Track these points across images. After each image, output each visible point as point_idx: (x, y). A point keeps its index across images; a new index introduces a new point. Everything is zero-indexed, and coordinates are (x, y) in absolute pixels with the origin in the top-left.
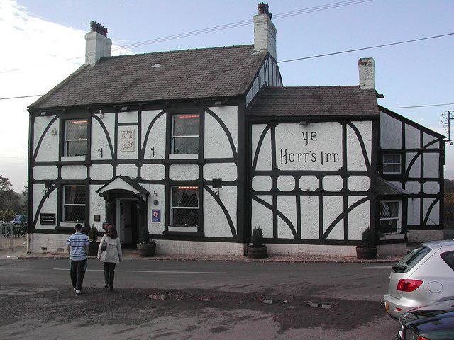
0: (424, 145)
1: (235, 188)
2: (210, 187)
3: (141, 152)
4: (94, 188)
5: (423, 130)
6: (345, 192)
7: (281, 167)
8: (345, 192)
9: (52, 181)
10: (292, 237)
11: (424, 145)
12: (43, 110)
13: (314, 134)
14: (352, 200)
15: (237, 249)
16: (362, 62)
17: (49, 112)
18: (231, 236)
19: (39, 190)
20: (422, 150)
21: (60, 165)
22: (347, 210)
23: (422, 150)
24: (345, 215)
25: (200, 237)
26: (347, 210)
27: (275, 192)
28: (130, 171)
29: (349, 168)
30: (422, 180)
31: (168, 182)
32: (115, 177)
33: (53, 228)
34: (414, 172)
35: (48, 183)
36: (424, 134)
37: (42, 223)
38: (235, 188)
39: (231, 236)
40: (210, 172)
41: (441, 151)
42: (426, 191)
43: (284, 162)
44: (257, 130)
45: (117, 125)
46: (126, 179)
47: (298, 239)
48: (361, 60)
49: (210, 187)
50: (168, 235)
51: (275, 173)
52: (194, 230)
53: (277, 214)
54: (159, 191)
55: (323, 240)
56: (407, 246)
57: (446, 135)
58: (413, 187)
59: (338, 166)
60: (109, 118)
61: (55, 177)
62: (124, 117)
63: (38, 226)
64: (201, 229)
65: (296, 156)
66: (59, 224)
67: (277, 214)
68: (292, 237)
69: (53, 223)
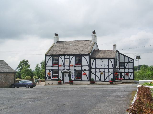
2: (84, 71)
3: (70, 64)
4: (60, 71)
5: (129, 58)
6: (109, 72)
8: (109, 72)
9: (51, 70)
12: (49, 55)
14: (110, 73)
15: (89, 82)
16: (114, 46)
17: (50, 55)
18: (87, 80)
19: (47, 72)
20: (129, 62)
21: (52, 66)
22: (109, 75)
23: (129, 62)
24: (109, 76)
25: (81, 80)
26: (109, 75)
27: (96, 72)
28: (68, 68)
29: (109, 67)
30: (129, 69)
31: (75, 70)
32: (64, 69)
33: (51, 79)
34: (127, 67)
35: (49, 70)
37: (48, 78)
38: (88, 71)
39: (87, 80)
40: (83, 68)
41: (133, 62)
42: (130, 71)
44: (92, 60)
45: (65, 59)
46: (67, 69)
47: (100, 81)
48: (113, 45)
49: (84, 71)
50: (75, 80)
51: (96, 68)
52: (81, 79)
53: (96, 76)
54: (73, 72)
55: (105, 81)
57: (134, 59)
59: (107, 67)
60: (63, 57)
61: (51, 69)
62: (66, 57)
63: (47, 79)
64: (82, 79)
66: (52, 78)
67: (96, 76)
69: (51, 78)
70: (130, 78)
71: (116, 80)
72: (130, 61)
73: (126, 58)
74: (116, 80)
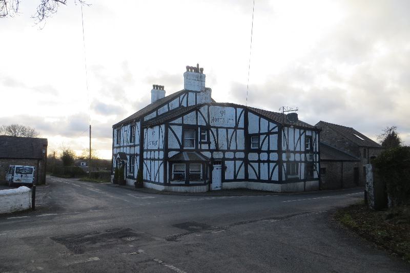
0: (270, 129)
7: (211, 124)
10: (256, 178)
11: (270, 129)
20: (269, 133)
23: (269, 133)
30: (269, 152)
33: (184, 183)
34: (265, 148)
36: (271, 123)
42: (271, 159)
44: (145, 130)
47: (259, 180)
56: (44, 143)
58: (264, 157)
68: (256, 178)
70: (273, 179)
71: (191, 182)
72: (272, 129)
73: (264, 122)
74: (191, 182)
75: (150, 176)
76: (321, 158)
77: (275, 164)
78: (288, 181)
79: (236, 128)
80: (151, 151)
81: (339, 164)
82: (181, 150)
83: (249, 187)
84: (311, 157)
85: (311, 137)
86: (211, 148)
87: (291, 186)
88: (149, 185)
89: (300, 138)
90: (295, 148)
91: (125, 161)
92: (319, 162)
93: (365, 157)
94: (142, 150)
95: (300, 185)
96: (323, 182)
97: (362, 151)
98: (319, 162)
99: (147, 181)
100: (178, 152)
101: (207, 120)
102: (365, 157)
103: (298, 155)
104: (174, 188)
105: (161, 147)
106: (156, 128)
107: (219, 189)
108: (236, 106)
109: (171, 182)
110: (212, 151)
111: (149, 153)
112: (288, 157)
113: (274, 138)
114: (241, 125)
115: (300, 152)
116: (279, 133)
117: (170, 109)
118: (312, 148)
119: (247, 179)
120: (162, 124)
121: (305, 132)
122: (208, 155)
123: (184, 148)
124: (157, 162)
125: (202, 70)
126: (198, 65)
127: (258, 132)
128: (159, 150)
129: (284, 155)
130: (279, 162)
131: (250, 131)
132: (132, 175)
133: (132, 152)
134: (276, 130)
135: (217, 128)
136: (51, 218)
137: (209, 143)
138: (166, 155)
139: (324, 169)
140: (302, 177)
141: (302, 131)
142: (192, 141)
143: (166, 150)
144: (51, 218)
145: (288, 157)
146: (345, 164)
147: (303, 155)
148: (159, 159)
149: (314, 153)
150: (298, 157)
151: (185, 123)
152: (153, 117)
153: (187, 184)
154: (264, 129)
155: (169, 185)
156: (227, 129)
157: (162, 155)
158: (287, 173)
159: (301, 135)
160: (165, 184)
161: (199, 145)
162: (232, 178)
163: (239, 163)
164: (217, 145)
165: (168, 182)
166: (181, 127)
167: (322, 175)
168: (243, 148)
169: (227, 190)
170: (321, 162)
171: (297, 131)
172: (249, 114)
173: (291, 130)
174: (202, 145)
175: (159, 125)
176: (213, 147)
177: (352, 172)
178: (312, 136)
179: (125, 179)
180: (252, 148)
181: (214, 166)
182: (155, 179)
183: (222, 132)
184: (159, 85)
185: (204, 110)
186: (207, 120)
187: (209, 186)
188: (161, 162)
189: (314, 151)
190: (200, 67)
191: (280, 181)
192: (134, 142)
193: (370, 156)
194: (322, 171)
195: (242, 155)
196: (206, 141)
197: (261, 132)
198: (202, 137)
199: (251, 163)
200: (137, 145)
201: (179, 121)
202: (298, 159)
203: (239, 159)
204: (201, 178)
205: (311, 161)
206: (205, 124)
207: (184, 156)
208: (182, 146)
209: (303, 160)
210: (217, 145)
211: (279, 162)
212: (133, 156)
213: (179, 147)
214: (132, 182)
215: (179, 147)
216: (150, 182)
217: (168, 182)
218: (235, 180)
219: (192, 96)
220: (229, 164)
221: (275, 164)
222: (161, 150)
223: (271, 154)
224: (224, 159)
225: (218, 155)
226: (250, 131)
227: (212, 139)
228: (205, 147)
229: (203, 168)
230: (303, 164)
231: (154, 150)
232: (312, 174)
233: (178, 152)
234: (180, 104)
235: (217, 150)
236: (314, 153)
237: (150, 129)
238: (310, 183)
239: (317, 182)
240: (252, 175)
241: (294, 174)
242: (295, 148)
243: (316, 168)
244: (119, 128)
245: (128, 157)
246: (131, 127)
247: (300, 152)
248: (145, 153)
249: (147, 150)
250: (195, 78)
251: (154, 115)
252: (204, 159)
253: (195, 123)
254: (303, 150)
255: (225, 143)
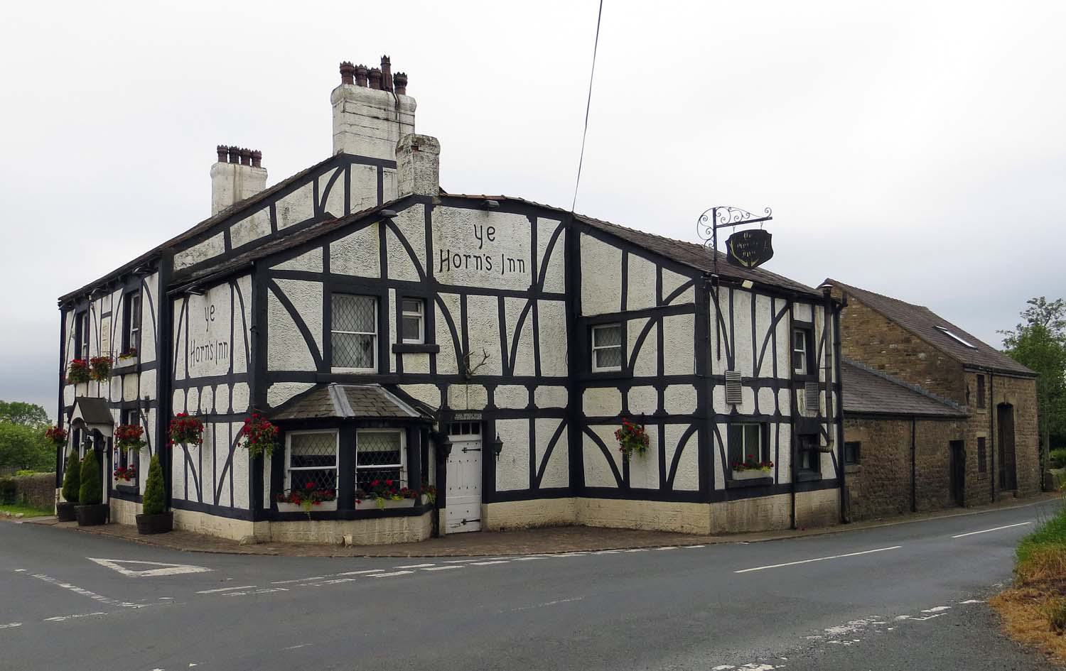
0: (664, 297)
1: (537, 420)
7: (440, 277)
13: (491, 231)
30: (661, 382)
34: (645, 366)
42: (670, 409)
43: (445, 268)
44: (178, 305)
65: (463, 259)
71: (365, 505)
73: (642, 268)
74: (365, 505)
75: (187, 457)
76: (847, 406)
77: (685, 427)
78: (736, 491)
79: (535, 293)
80: (200, 383)
81: (903, 429)
82: (322, 378)
83: (584, 519)
84: (813, 402)
85: (808, 330)
86: (440, 371)
87: (743, 506)
88: (192, 520)
89: (772, 331)
90: (757, 370)
91: (105, 431)
92: (838, 420)
93: (981, 405)
94: (166, 384)
95: (777, 504)
96: (854, 494)
97: (971, 381)
98: (838, 420)
99: (185, 505)
100: (305, 387)
101: (423, 263)
102: (981, 405)
103: (766, 393)
104: (291, 530)
105: (241, 367)
106: (221, 294)
107: (473, 527)
108: (534, 211)
109: (283, 507)
110: (443, 382)
111: (193, 391)
112: (733, 400)
113: (680, 329)
114: (555, 281)
115: (775, 384)
116: (700, 310)
117: (280, 226)
118: (813, 368)
119: (577, 487)
120: (242, 272)
121: (789, 307)
122: (429, 395)
123: (335, 370)
124: (222, 428)
125: (401, 81)
126: (386, 61)
127: (618, 310)
128: (231, 379)
129: (719, 393)
130: (702, 421)
131: (589, 308)
132: (131, 483)
133: (131, 397)
134: (689, 296)
135: (464, 292)
136: (693, 261)
137: (431, 349)
138: (258, 396)
139: (855, 446)
140: (784, 477)
141: (780, 304)
142: (367, 345)
143: (260, 377)
144: (693, 261)
145: (733, 400)
146: (921, 426)
147: (784, 393)
148: (230, 417)
149: (823, 386)
150: (767, 402)
151: (336, 268)
152: (211, 254)
153: (347, 513)
154: (642, 297)
155: (273, 516)
156: (501, 295)
157: (241, 398)
158: (734, 463)
159: (775, 320)
160: (257, 513)
161: (393, 358)
162: (524, 484)
163: (547, 427)
164: (463, 356)
165: (267, 505)
166: (319, 286)
167: (848, 468)
168: (562, 371)
169: (503, 532)
170: (844, 422)
171: (763, 302)
172: (586, 240)
173: (742, 300)
174: (405, 357)
175: (230, 278)
176: (447, 365)
177: (943, 455)
178: (812, 324)
179: (105, 501)
180: (596, 369)
181: (452, 438)
182: (217, 499)
183: (482, 311)
184: (241, 146)
185: (410, 222)
186: (423, 263)
187: (436, 520)
188: (238, 426)
189: (823, 378)
190: (394, 70)
191: (705, 494)
192: (136, 353)
193: (998, 400)
194: (850, 453)
195: (557, 397)
196: (420, 341)
197: (629, 308)
198: (405, 327)
199: (593, 428)
200: (149, 366)
201: (310, 260)
202: (767, 409)
203: (550, 413)
204: (404, 485)
205: (813, 415)
206: (414, 277)
207: (334, 401)
208: (324, 363)
209: (786, 412)
210: (463, 356)
211: (702, 421)
212: (131, 410)
213: (311, 366)
214: (129, 512)
215: (311, 366)
216: (200, 507)
217: (267, 505)
218: (534, 491)
219: (363, 178)
220: (511, 432)
221: (685, 427)
222: (241, 378)
223: (670, 390)
224: (493, 413)
225: (466, 399)
226: (589, 308)
227: (443, 337)
228: (416, 364)
229: (409, 449)
230: (785, 428)
231: (214, 382)
232: (815, 465)
233: (305, 387)
234: (319, 209)
235: (465, 377)
236: (823, 386)
237: (196, 301)
238: (822, 499)
239: (831, 495)
240: (598, 473)
241: (752, 465)
242: (757, 370)
243: (829, 441)
244: (83, 307)
245: (116, 414)
246: (127, 298)
247: (775, 384)
248: (178, 395)
249: (187, 384)
250: (375, 112)
251: (214, 246)
252: (413, 413)
253: (374, 273)
254: (784, 374)
255: (495, 350)
